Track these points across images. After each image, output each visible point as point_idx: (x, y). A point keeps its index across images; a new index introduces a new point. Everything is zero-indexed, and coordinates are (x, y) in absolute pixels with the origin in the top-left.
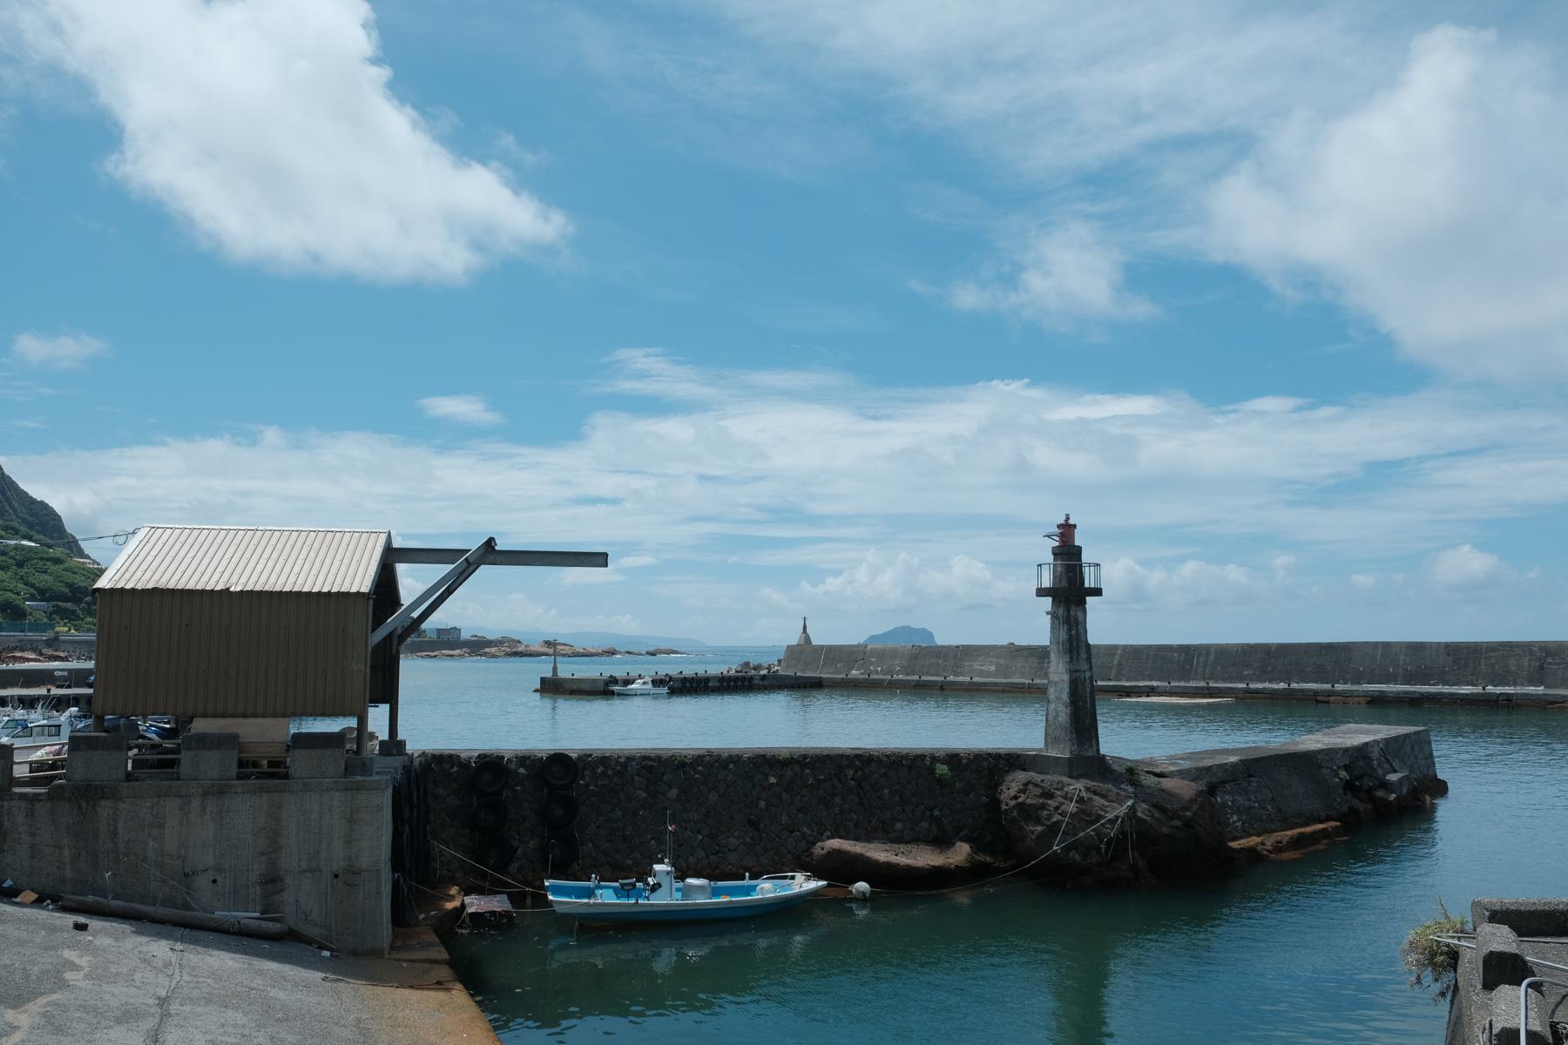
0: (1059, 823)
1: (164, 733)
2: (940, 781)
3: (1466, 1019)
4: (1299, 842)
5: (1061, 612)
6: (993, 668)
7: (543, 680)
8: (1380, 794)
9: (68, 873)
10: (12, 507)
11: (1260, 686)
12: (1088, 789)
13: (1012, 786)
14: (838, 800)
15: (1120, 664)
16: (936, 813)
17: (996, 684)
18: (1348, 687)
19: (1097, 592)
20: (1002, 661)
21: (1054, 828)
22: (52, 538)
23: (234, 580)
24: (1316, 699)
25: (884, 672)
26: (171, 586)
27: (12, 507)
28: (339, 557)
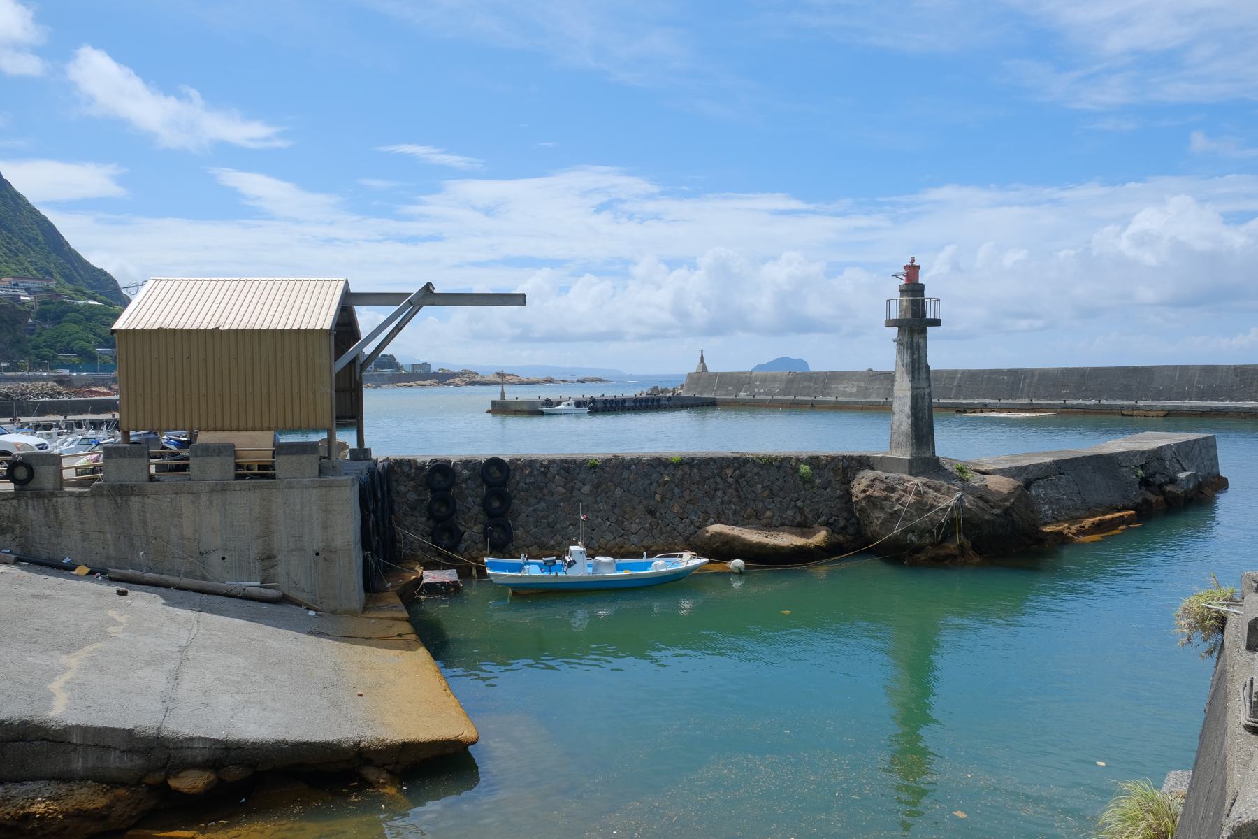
0: (900, 510)
1: (181, 444)
2: (805, 480)
3: (1229, 675)
4: (1098, 528)
5: (906, 339)
6: (854, 390)
7: (494, 403)
8: (1169, 488)
9: (112, 552)
10: (79, 274)
11: (1075, 402)
12: (924, 484)
13: (861, 483)
14: (719, 493)
15: (959, 386)
16: (799, 503)
17: (856, 402)
18: (1149, 403)
19: (936, 322)
20: (862, 384)
21: (895, 516)
22: (112, 298)
23: (222, 321)
24: (1122, 413)
25: (766, 394)
26: (172, 326)
27: (79, 274)
28: (306, 301)
